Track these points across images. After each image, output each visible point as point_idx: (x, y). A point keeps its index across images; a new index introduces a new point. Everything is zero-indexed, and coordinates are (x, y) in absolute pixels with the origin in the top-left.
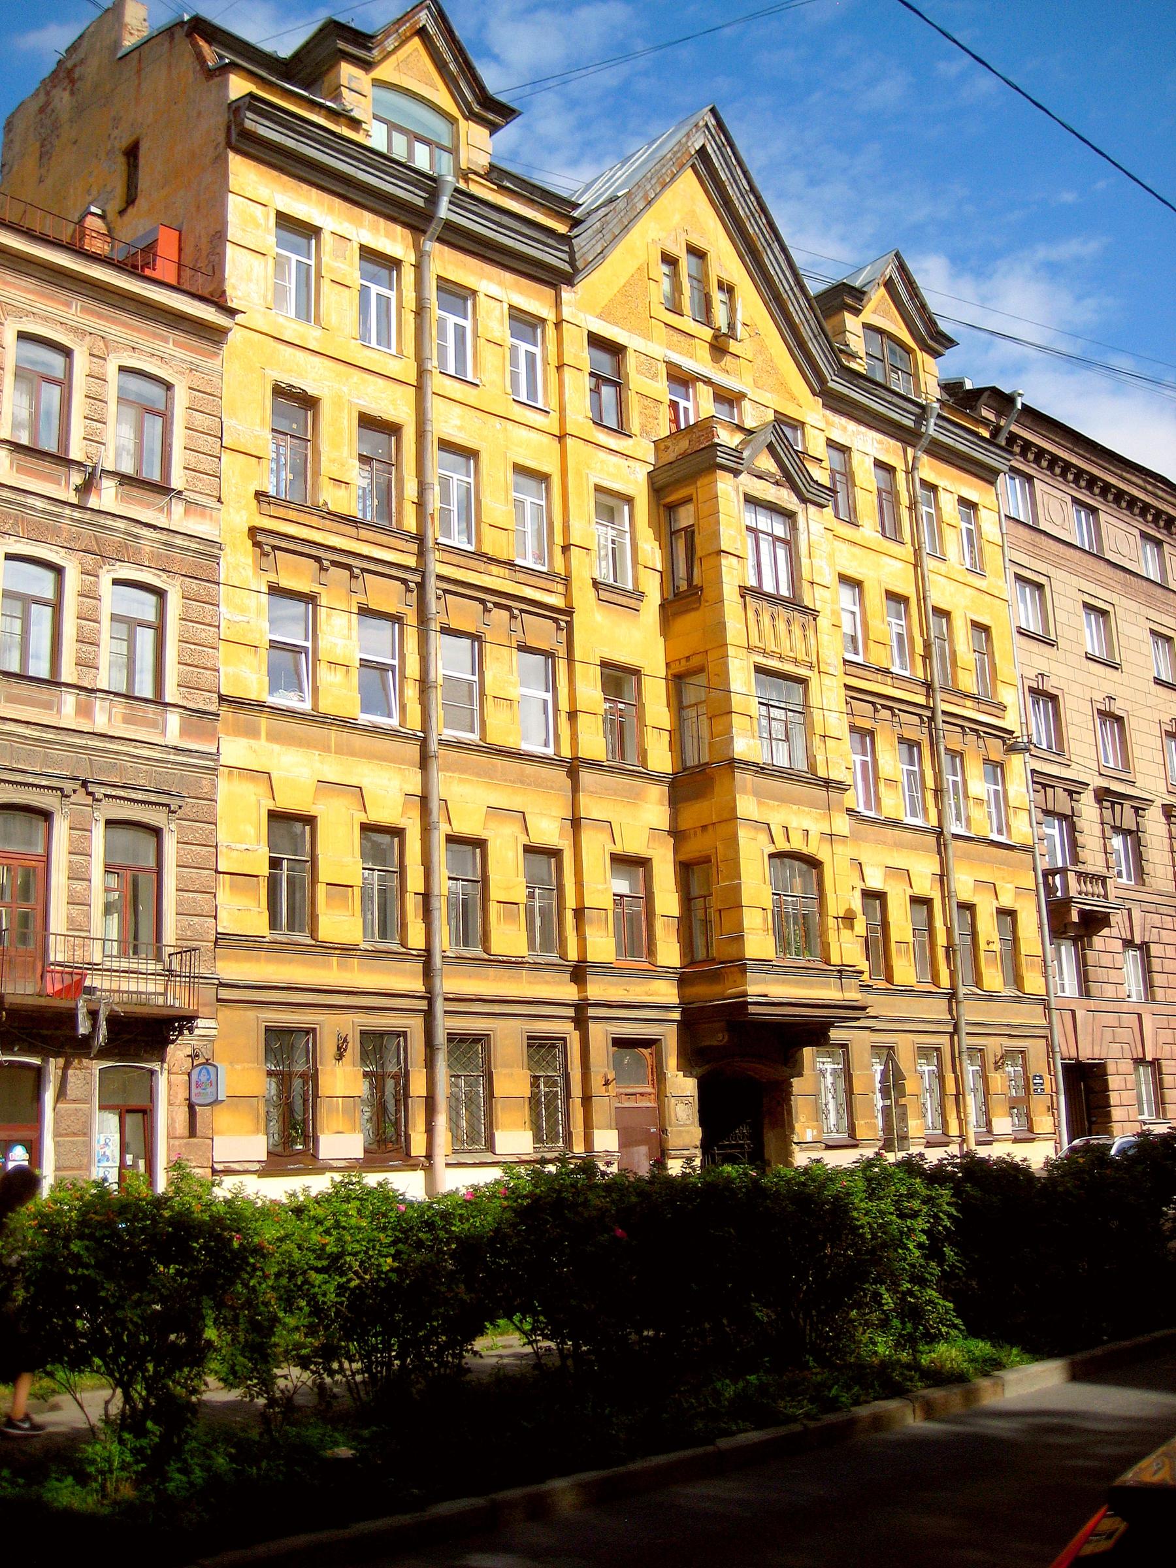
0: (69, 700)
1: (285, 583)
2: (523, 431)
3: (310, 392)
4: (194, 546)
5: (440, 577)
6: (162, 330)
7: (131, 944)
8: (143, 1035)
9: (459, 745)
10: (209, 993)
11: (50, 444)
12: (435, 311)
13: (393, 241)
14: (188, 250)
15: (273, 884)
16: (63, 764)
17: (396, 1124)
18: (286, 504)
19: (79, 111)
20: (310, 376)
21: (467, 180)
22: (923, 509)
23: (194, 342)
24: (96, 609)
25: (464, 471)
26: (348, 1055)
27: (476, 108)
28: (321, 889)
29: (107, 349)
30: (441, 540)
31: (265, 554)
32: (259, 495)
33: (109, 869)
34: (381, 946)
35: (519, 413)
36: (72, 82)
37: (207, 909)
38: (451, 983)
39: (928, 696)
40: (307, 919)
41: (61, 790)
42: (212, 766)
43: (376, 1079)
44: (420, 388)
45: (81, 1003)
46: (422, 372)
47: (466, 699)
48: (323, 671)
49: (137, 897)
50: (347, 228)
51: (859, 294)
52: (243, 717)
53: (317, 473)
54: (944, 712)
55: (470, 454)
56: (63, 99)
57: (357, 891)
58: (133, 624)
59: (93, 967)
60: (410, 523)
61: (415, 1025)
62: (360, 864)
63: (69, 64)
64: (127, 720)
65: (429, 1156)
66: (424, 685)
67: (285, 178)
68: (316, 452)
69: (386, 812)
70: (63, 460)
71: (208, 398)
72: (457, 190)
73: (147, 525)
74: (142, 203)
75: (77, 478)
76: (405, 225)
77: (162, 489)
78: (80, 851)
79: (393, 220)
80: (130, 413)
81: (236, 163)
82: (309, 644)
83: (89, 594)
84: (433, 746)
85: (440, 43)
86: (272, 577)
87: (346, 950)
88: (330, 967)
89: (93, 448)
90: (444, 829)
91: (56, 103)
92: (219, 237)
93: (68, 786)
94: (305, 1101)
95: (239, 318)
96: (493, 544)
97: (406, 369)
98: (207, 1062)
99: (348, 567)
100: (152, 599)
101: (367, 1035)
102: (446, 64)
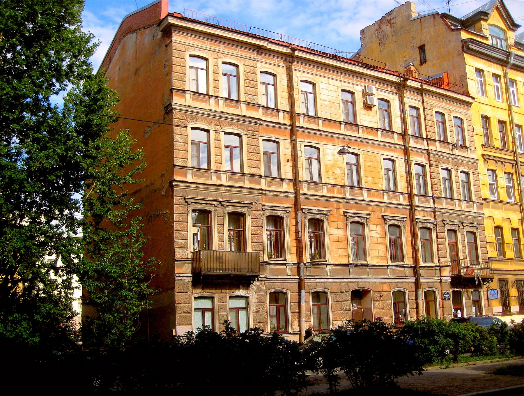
0: (457, 202)
1: (490, 168)
4: (473, 161)
13: (498, 70)
16: (457, 219)
21: (511, 48)
22: (511, 89)
27: (511, 27)
28: (505, 245)
31: (485, 161)
32: (482, 145)
37: (486, 252)
39: (514, 156)
41: (286, 211)
51: (486, 14)
53: (492, 137)
54: (521, 162)
58: (231, 148)
79: (498, 64)
81: (466, 56)
82: (495, 183)
85: (501, 10)
87: (511, 260)
97: (505, 106)
100: (205, 133)
102: (503, 16)
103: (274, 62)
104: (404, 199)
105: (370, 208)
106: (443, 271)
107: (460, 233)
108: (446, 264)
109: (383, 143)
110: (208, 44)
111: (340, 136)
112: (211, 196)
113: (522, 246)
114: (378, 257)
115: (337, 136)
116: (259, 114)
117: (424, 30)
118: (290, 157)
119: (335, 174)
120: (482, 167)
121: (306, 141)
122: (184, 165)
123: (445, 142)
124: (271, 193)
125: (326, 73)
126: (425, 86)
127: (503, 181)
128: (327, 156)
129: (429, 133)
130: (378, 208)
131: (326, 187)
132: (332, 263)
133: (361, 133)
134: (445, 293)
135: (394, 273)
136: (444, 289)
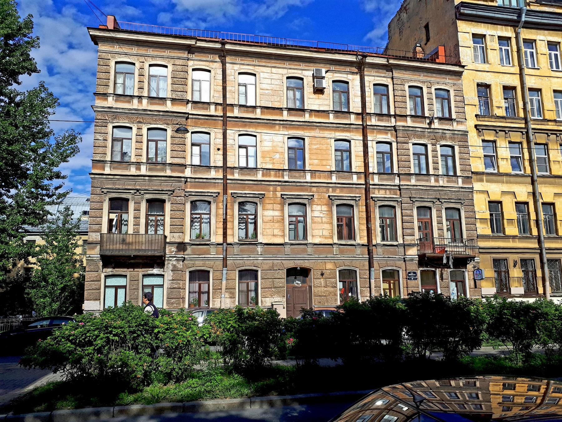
1: (487, 138)
2: (556, 79)
3: (488, 83)
4: (460, 133)
5: (533, 129)
6: (444, 76)
7: (454, 239)
8: (461, 262)
9: (543, 177)
10: (477, 251)
11: (420, 114)
12: (523, 49)
13: (508, 32)
14: (448, 51)
15: (491, 220)
16: (432, 195)
17: (533, 285)
18: (484, 116)
19: (409, 18)
20: (486, 79)
21: (529, 6)
23: (454, 77)
24: (437, 154)
25: (537, 95)
26: (517, 265)
28: (505, 221)
29: (431, 85)
30: (532, 118)
31: (480, 132)
32: (476, 116)
33: (447, 220)
34: (524, 235)
35: (554, 74)
36: (406, 10)
38: (547, 245)
40: (502, 229)
42: (472, 191)
43: (526, 272)
44: (521, 75)
45: (445, 255)
46: (521, 69)
47: (544, 162)
48: (500, 160)
49: (455, 227)
50: (492, 32)
52: (479, 177)
53: (492, 106)
55: (539, 90)
56: (404, 16)
57: (516, 221)
59: (446, 245)
60: (522, 115)
61: (537, 257)
62: (516, 213)
63: (405, 6)
64: (448, 182)
65: (545, 293)
66: (531, 161)
67: (473, 23)
68: (491, 100)
69: (523, 197)
70: (423, 117)
71: (459, 92)
72: (528, 11)
73: (447, 130)
74: (431, 40)
75: (428, 121)
76: (511, 26)
77: (450, 119)
78: (439, 216)
79: (507, 25)
80: (439, 100)
81: (459, 23)
82: (495, 154)
83: (434, 151)
84: (535, 178)
86: (483, 138)
87: (514, 237)
88: (510, 242)
89: (431, 112)
90: (541, 201)
91: (402, 17)
92: (457, 46)
93: (435, 201)
94: (506, 279)
95: (465, 68)
96: (548, 115)
97: (516, 70)
98: (478, 269)
99: (504, 131)
101: (522, 260)
103: (208, 59)
104: (359, 178)
105: (314, 189)
106: (408, 250)
107: (435, 210)
108: (413, 242)
109: (335, 125)
110: (135, 50)
111: (282, 122)
112: (129, 185)
113: (559, 223)
114: (322, 236)
115: (278, 122)
116: (188, 109)
117: (428, 7)
118: (221, 147)
119: (273, 159)
120: (474, 139)
121: (240, 129)
122: (102, 159)
123: (419, 117)
124: (197, 180)
125: (269, 63)
126: (391, 61)
127: (504, 151)
128: (265, 142)
129: (397, 110)
130: (325, 189)
131: (261, 172)
132: (264, 242)
133: (307, 117)
134: (409, 273)
135: (341, 252)
136: (408, 268)
